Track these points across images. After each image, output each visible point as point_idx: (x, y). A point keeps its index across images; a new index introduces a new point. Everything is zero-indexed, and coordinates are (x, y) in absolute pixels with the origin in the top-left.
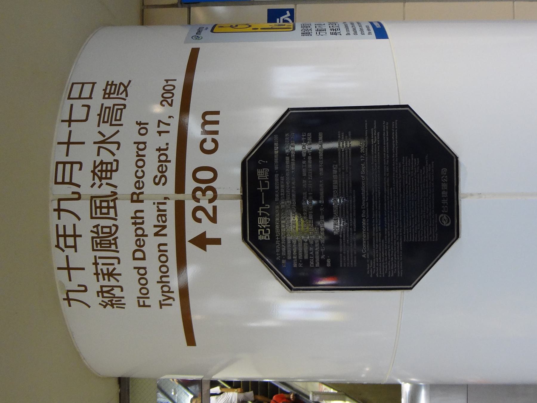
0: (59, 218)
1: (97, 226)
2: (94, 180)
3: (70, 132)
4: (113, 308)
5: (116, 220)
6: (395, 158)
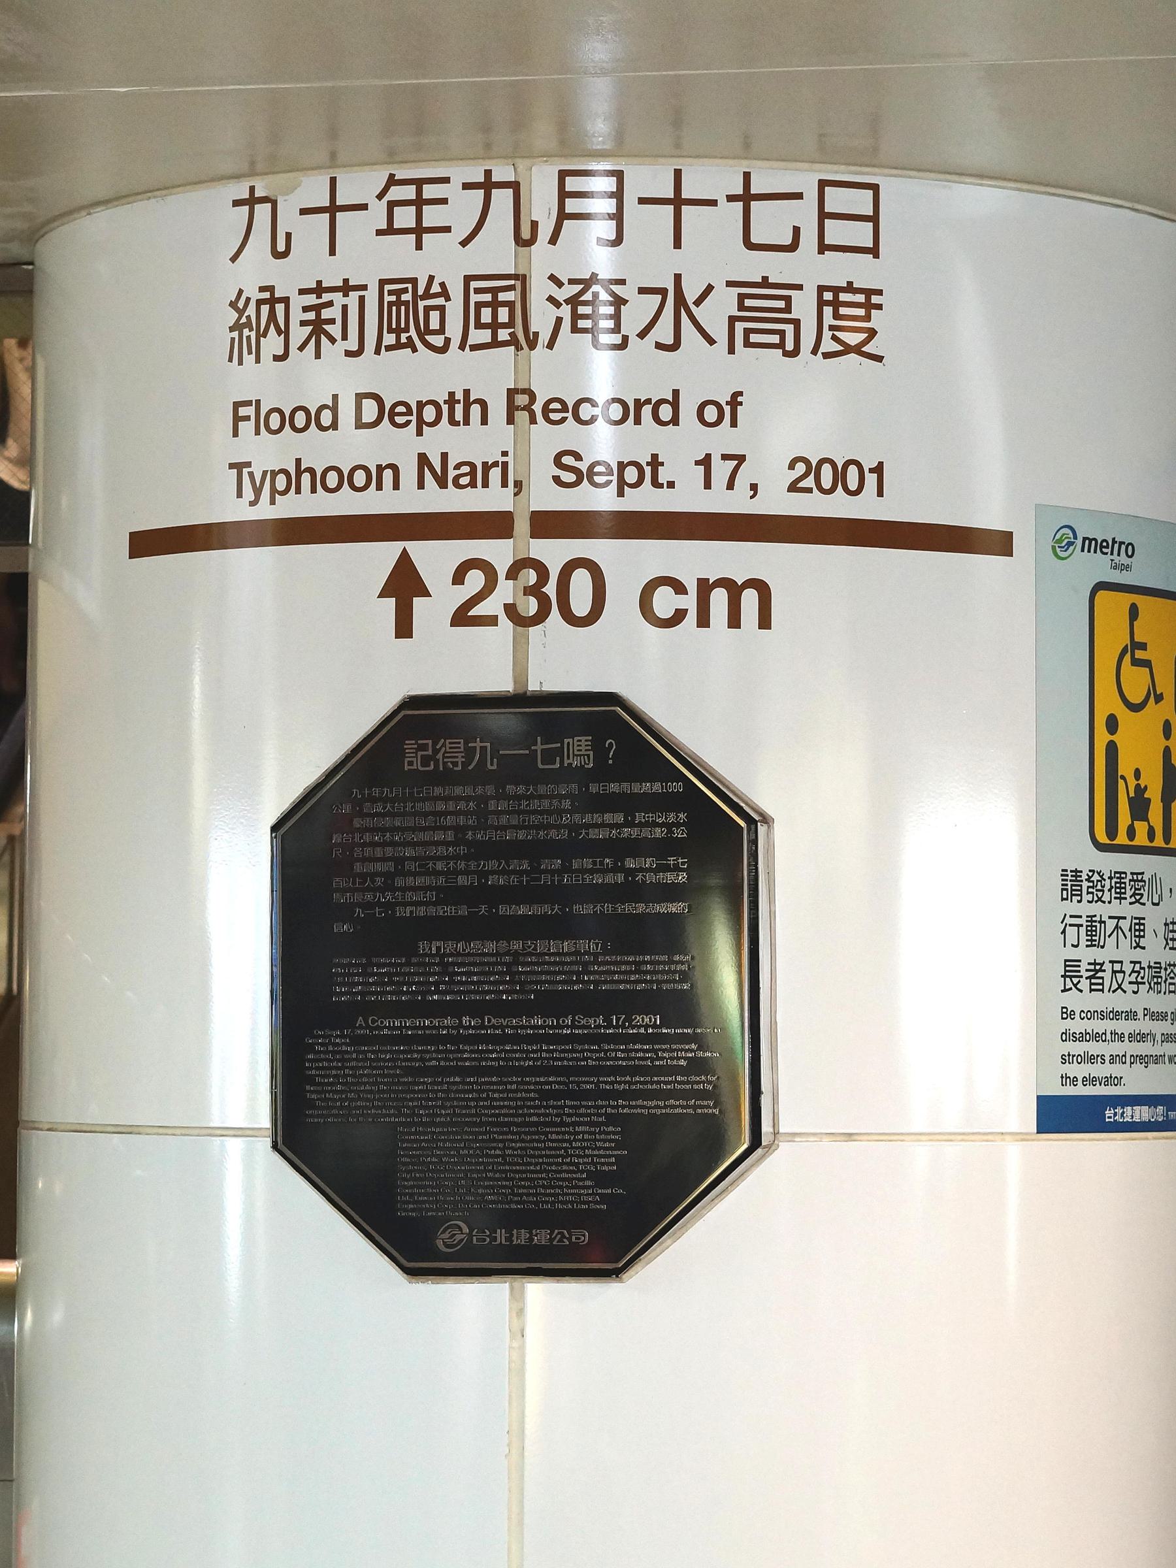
0: (467, 186)
1: (445, 293)
2: (572, 282)
3: (713, 203)
4: (231, 329)
5: (462, 347)
6: (617, 1107)
